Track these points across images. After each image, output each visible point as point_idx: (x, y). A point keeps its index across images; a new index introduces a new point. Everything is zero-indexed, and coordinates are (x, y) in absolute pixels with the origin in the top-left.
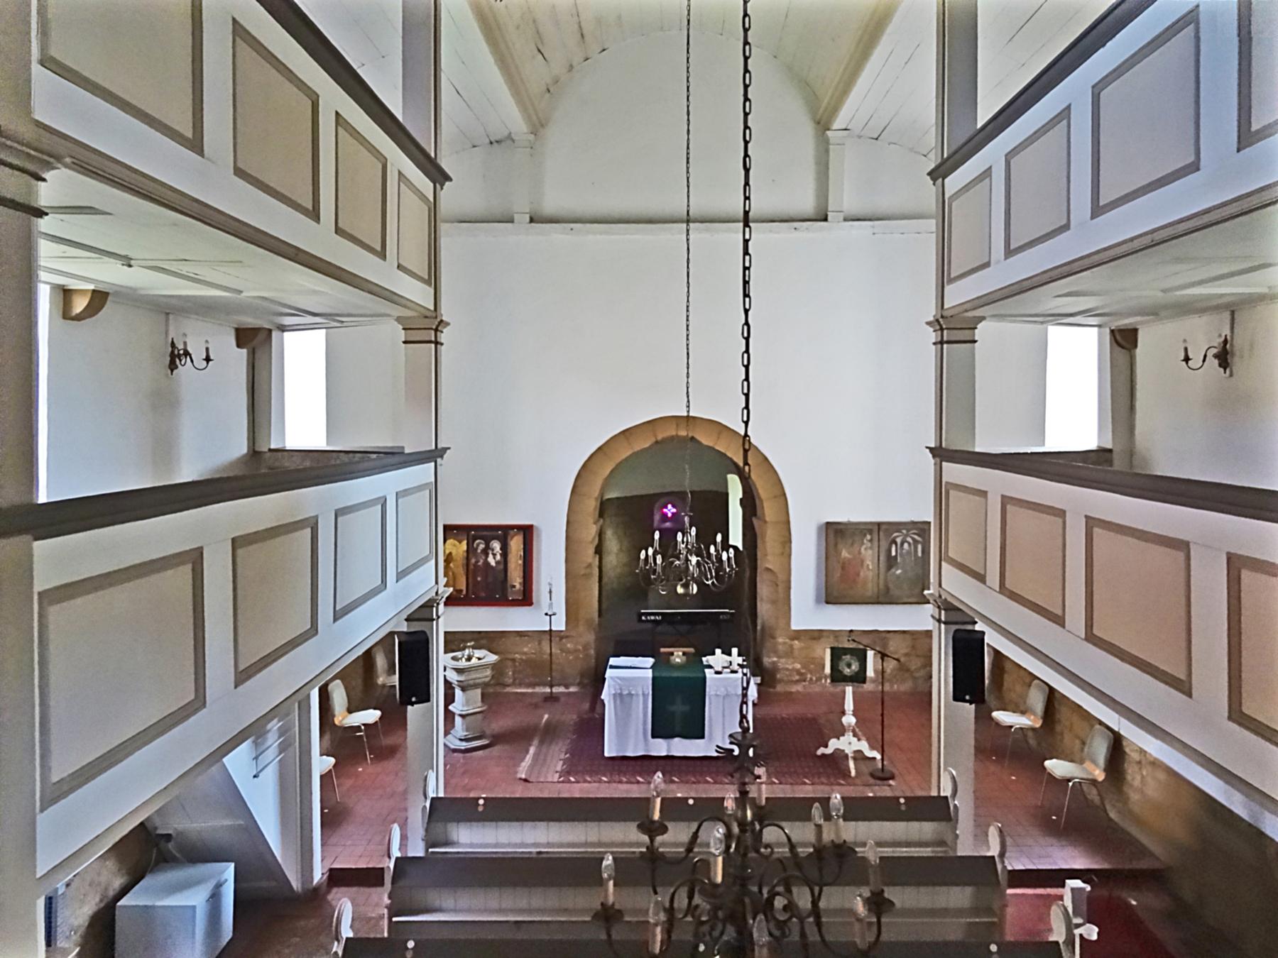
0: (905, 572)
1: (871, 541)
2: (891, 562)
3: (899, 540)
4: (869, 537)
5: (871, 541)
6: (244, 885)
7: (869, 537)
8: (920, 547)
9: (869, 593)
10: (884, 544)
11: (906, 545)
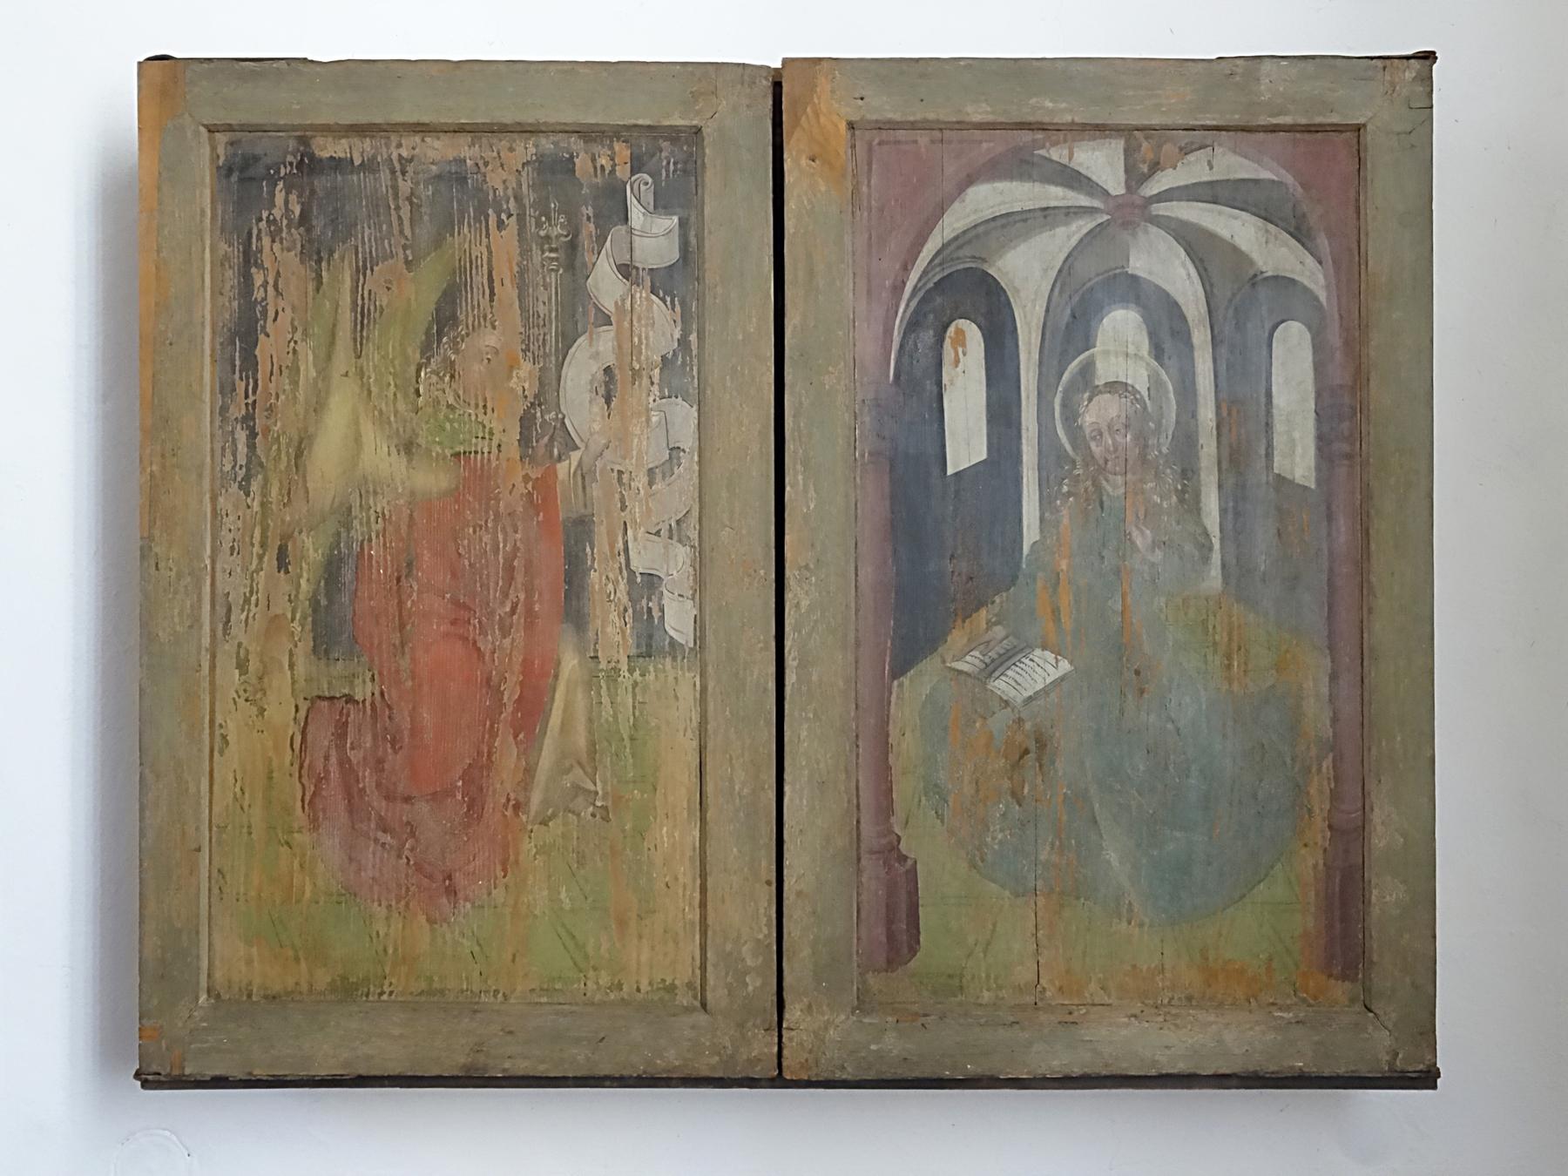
0: (1119, 665)
1: (678, 280)
2: (938, 557)
3: (1027, 272)
4: (653, 235)
5: (678, 280)
6: (824, 85)
7: (653, 235)
8: (1292, 369)
9: (657, 958)
10: (845, 329)
11: (1121, 328)
